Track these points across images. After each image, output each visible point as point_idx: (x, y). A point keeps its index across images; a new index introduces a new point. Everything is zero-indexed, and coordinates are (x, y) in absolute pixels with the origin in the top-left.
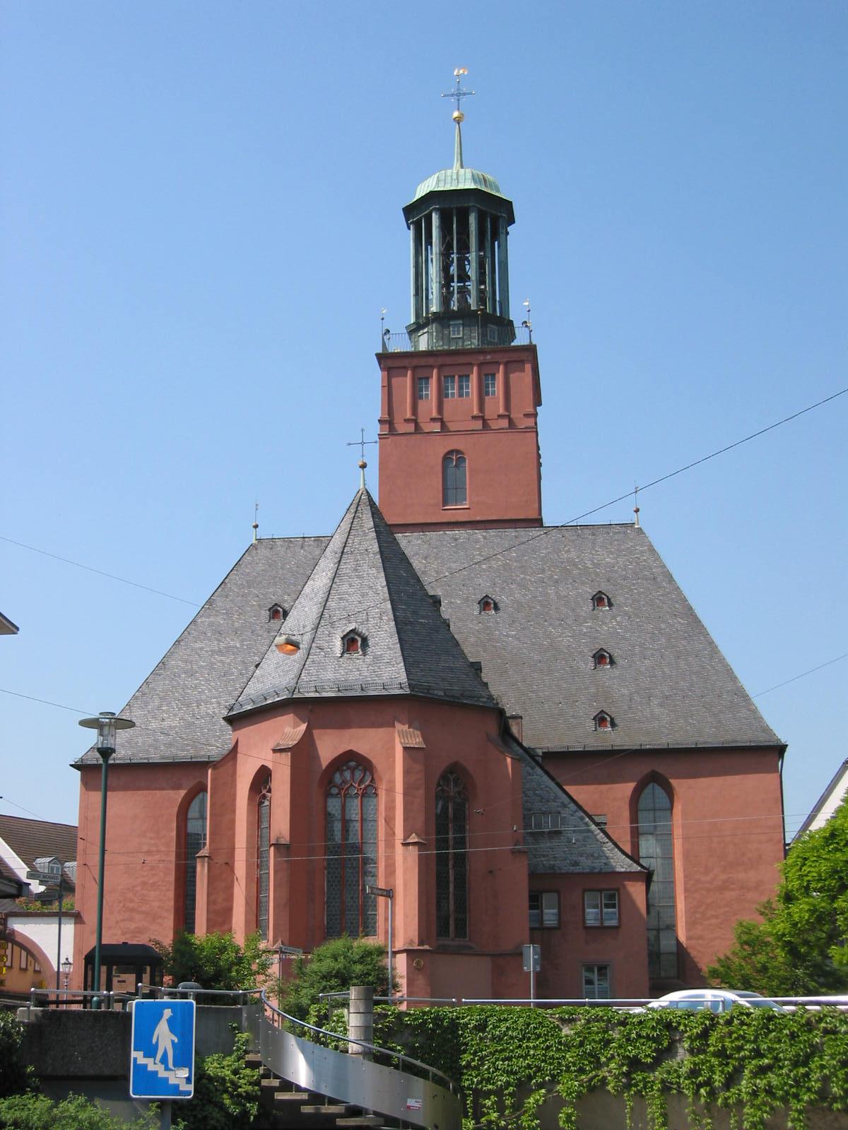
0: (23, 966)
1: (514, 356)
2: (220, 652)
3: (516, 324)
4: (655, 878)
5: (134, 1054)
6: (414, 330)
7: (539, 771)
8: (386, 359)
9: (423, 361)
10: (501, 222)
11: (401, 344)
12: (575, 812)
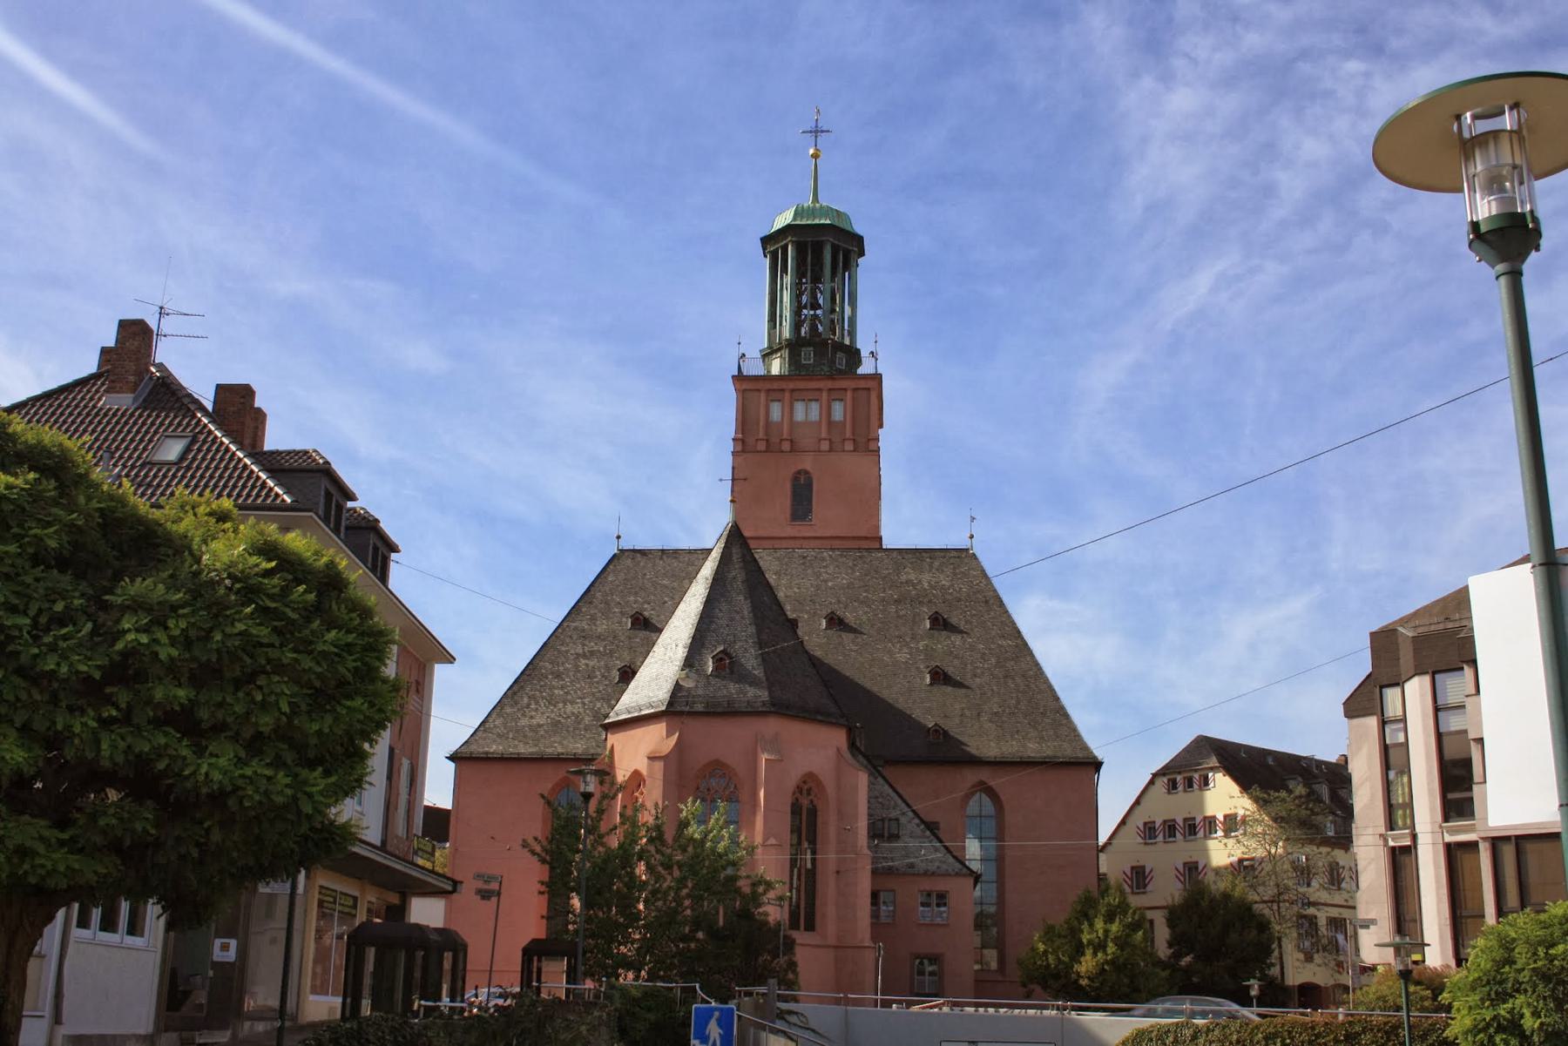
1: (862, 384)
2: (584, 656)
6: (767, 355)
8: (739, 378)
9: (776, 385)
10: (853, 256)
11: (754, 368)
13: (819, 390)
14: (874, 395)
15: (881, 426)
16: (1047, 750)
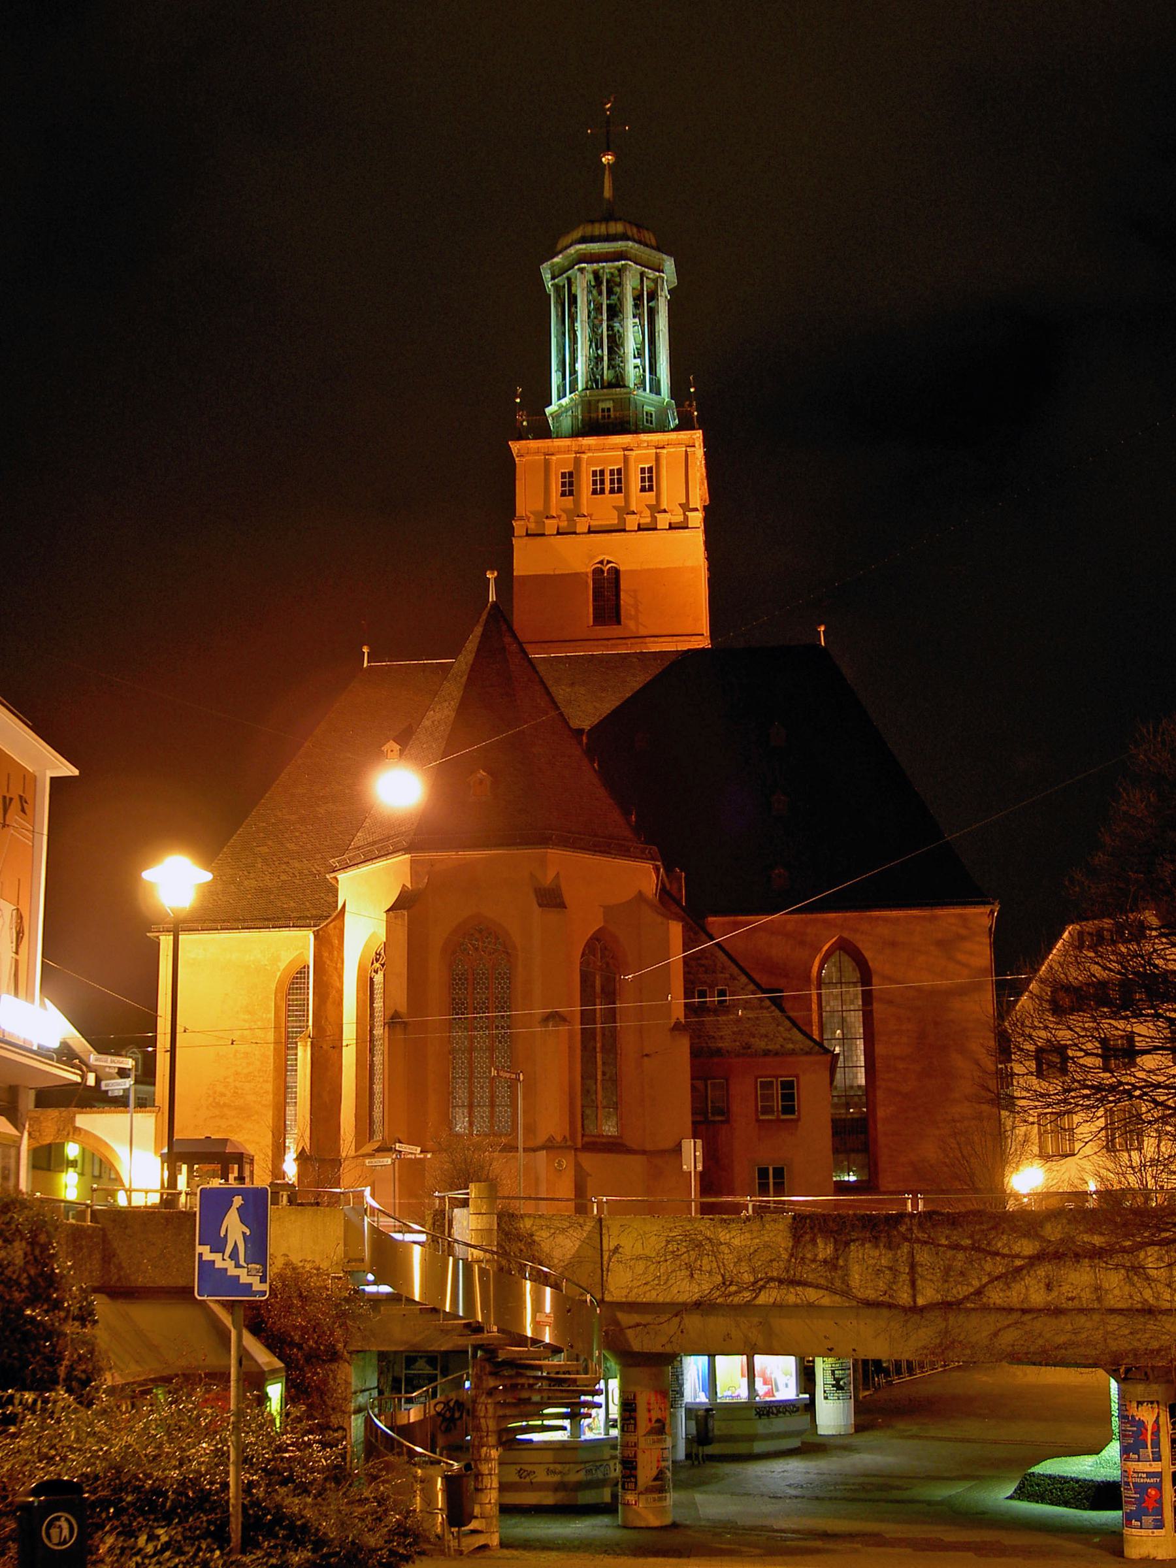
0: (97, 1173)
5: (199, 1249)
12: (746, 985)
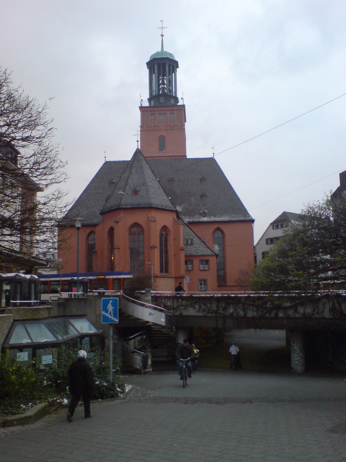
3: (179, 99)
4: (218, 256)
7: (187, 227)
13: (166, 110)
14: (183, 111)
15: (185, 122)
16: (242, 218)
